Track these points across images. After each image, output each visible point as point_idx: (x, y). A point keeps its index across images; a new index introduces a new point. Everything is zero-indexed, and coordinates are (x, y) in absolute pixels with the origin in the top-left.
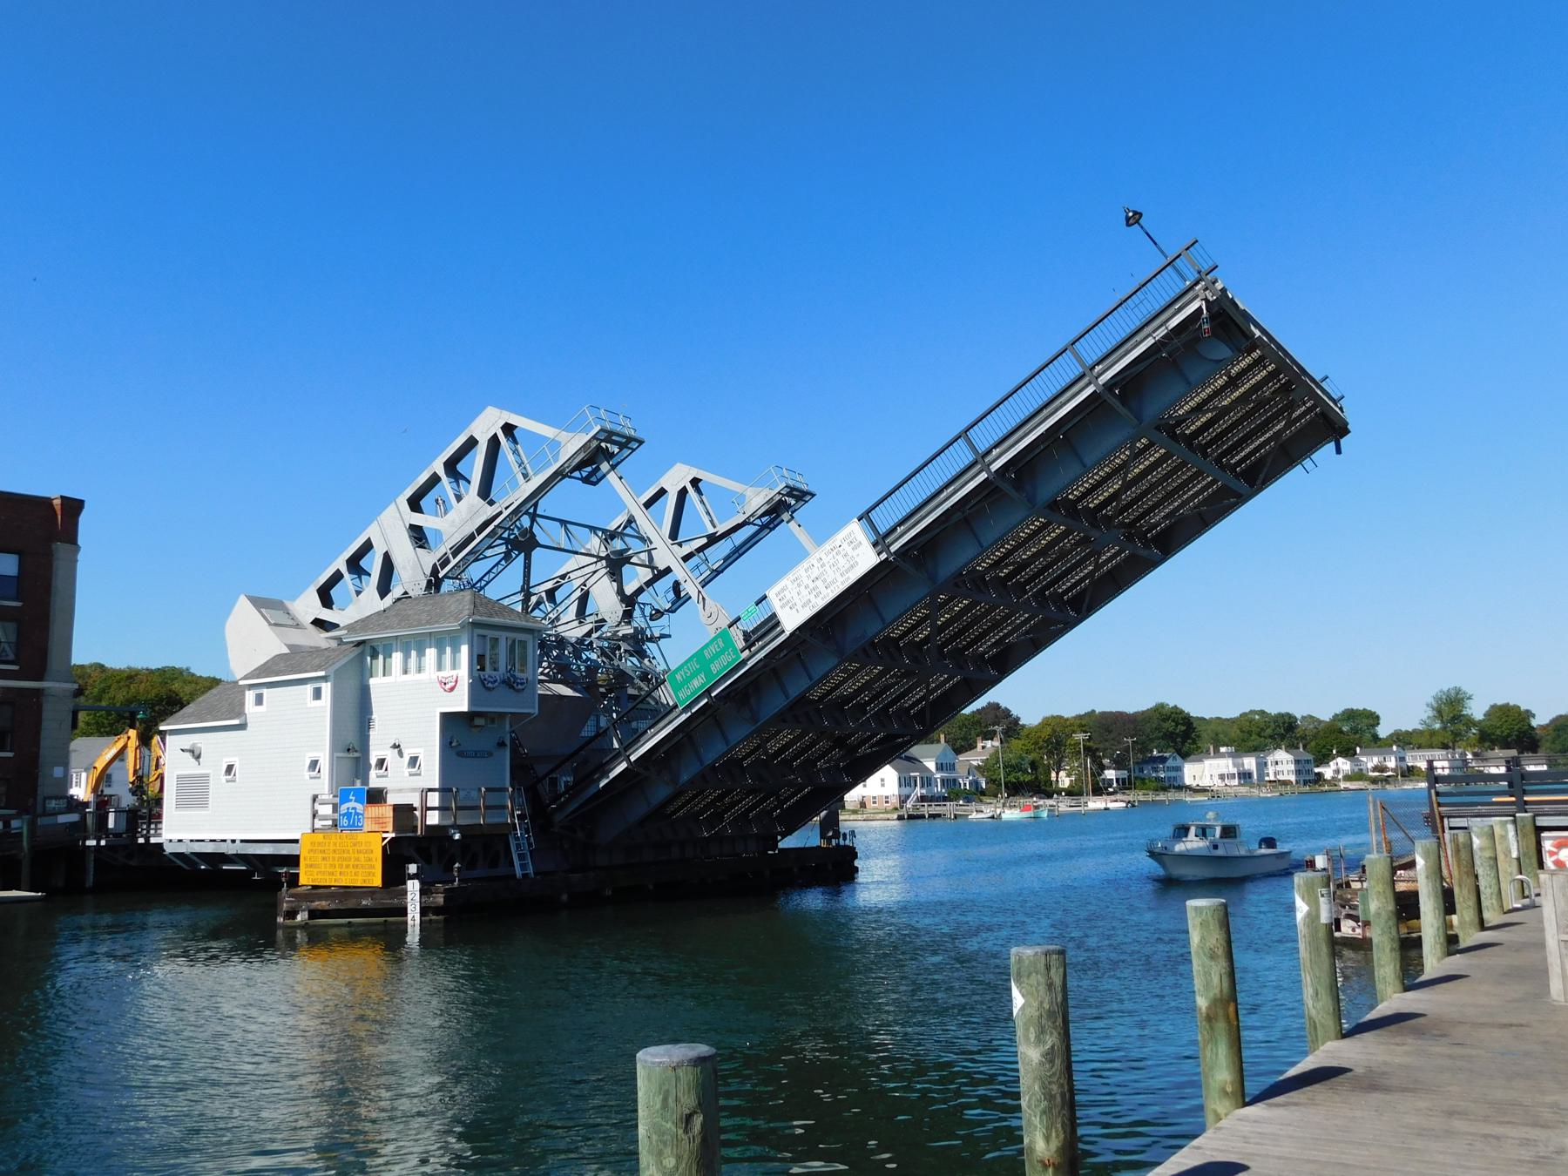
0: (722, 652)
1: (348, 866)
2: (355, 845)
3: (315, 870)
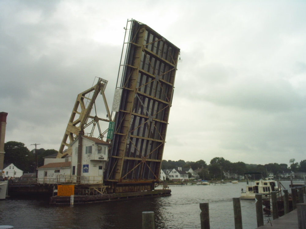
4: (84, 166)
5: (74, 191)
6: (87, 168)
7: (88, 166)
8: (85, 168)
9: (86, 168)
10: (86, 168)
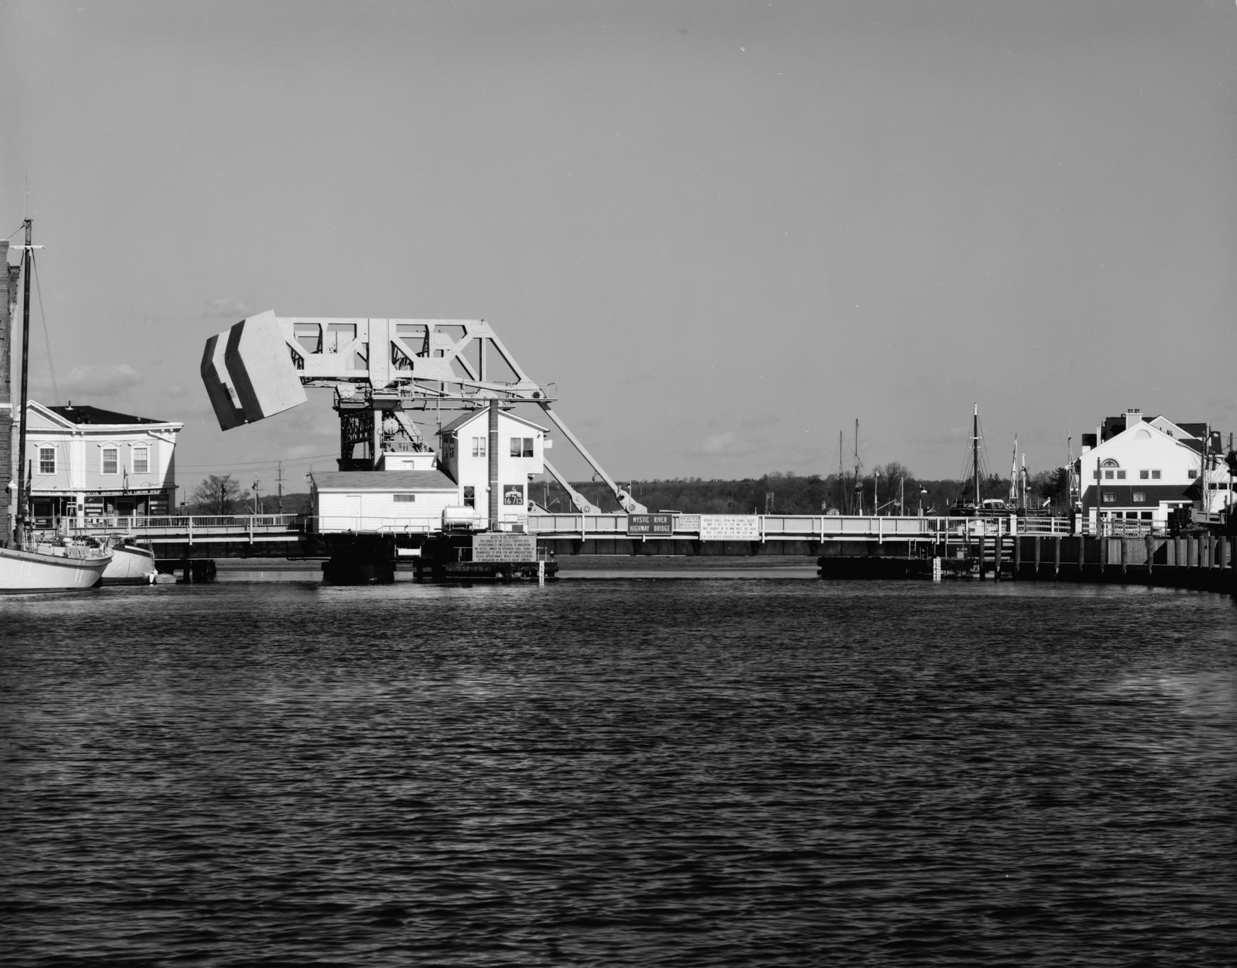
0: (664, 524)
1: (510, 552)
2: (516, 541)
3: (485, 555)
4: (507, 488)
5: (535, 550)
6: (519, 494)
7: (520, 489)
8: (508, 494)
9: (514, 492)
10: (514, 492)
